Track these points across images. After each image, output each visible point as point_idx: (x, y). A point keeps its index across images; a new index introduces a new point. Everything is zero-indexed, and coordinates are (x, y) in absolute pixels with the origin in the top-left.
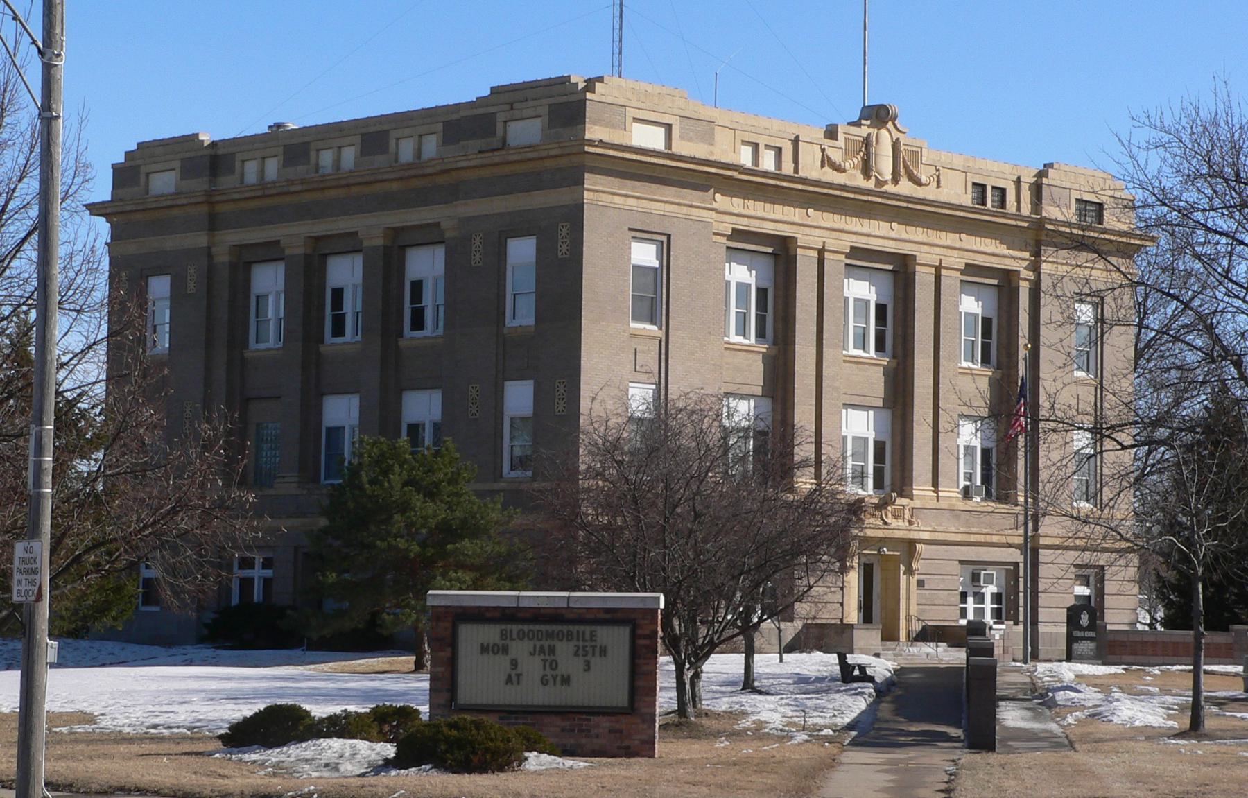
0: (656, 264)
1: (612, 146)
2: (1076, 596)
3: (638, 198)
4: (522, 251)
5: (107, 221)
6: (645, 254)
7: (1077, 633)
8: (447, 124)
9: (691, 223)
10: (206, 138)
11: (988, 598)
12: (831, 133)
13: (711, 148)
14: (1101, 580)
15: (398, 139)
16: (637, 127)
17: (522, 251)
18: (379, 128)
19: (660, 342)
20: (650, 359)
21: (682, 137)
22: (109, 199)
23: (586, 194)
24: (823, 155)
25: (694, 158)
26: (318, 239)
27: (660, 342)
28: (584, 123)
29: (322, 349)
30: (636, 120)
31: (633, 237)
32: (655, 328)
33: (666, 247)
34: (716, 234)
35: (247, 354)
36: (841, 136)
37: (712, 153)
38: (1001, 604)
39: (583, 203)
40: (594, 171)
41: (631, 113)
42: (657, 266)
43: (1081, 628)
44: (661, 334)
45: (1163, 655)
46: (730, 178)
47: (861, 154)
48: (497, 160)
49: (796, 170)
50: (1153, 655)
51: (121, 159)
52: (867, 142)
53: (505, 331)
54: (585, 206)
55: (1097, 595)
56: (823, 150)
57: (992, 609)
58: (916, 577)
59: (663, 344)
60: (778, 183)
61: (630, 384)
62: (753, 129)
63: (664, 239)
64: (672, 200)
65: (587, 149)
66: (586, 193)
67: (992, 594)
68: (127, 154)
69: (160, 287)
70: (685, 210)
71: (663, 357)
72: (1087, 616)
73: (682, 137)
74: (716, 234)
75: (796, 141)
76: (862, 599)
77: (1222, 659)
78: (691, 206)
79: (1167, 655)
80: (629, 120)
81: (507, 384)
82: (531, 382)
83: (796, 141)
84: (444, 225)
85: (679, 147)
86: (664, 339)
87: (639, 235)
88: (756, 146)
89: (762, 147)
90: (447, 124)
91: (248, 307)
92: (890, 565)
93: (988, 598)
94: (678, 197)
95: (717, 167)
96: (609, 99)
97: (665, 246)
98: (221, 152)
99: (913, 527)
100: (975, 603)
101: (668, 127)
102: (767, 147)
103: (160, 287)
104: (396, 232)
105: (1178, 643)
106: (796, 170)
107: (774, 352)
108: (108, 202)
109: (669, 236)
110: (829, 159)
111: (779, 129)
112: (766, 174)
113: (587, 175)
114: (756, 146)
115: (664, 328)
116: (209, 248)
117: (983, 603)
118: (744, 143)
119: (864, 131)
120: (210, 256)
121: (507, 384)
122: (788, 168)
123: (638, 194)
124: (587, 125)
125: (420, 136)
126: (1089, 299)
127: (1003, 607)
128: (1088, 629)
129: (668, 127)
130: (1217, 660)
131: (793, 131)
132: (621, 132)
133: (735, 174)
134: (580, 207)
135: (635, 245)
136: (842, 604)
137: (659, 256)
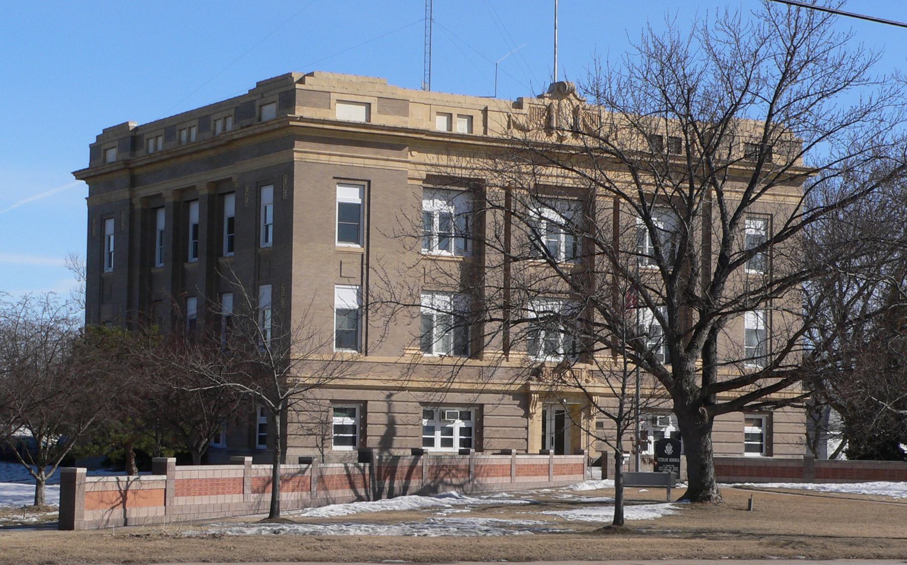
0: (359, 201)
1: (312, 121)
2: (746, 434)
3: (330, 155)
4: (267, 194)
5: (87, 183)
6: (349, 195)
7: (662, 460)
8: (236, 108)
9: (389, 171)
10: (133, 125)
11: (456, 432)
12: (518, 104)
13: (405, 119)
14: (364, 412)
15: (215, 121)
16: (339, 106)
17: (267, 194)
18: (205, 114)
19: (362, 255)
20: (354, 269)
21: (379, 112)
22: (88, 166)
23: (295, 155)
24: (509, 119)
25: (384, 126)
26: (183, 191)
27: (362, 255)
28: (294, 105)
29: (186, 266)
30: (339, 101)
31: (338, 183)
32: (358, 246)
33: (366, 187)
34: (410, 179)
35: (153, 271)
36: (526, 106)
37: (406, 122)
38: (471, 435)
39: (293, 161)
40: (303, 138)
41: (334, 97)
42: (360, 203)
43: (666, 456)
44: (363, 250)
45: (750, 476)
46: (421, 139)
47: (544, 118)
48: (251, 133)
49: (485, 132)
50: (742, 476)
51: (94, 141)
52: (549, 109)
53: (259, 251)
54: (295, 163)
55: (767, 434)
56: (509, 117)
57: (461, 439)
58: (595, 420)
59: (365, 257)
60: (464, 141)
61: (336, 286)
62: (447, 104)
63: (366, 184)
64: (371, 156)
65: (291, 123)
66: (295, 154)
67: (461, 428)
68: (98, 137)
69: (110, 225)
70: (382, 163)
71: (365, 266)
72: (671, 447)
73: (379, 112)
74: (410, 179)
75: (485, 111)
76: (554, 436)
77: (795, 479)
78: (387, 160)
79: (753, 476)
80: (333, 101)
81: (261, 287)
82: (270, 286)
83: (485, 111)
84: (235, 179)
85: (378, 119)
86: (365, 254)
87: (342, 181)
88: (450, 116)
89: (455, 117)
90: (236, 108)
91: (155, 238)
92: (575, 412)
93: (456, 432)
94: (377, 153)
95: (406, 132)
96: (315, 88)
97: (366, 188)
98: (138, 133)
99: (590, 384)
100: (442, 435)
101: (368, 106)
102: (459, 116)
103: (110, 225)
104: (217, 184)
105: (761, 467)
106: (485, 132)
107: (469, 261)
108: (87, 169)
109: (369, 182)
110: (514, 123)
111: (473, 103)
112: (462, 136)
113: (296, 142)
114: (450, 116)
115: (365, 246)
116: (131, 199)
117: (452, 435)
118: (439, 113)
119: (547, 101)
120: (132, 205)
121: (261, 287)
122: (478, 131)
123: (328, 152)
124: (296, 107)
125: (225, 118)
126: (762, 216)
127: (764, 443)
128: (672, 456)
129: (368, 106)
130: (845, 480)
131: (484, 103)
132: (326, 110)
133: (423, 136)
134: (292, 163)
135: (339, 188)
136: (527, 440)
137: (362, 196)
